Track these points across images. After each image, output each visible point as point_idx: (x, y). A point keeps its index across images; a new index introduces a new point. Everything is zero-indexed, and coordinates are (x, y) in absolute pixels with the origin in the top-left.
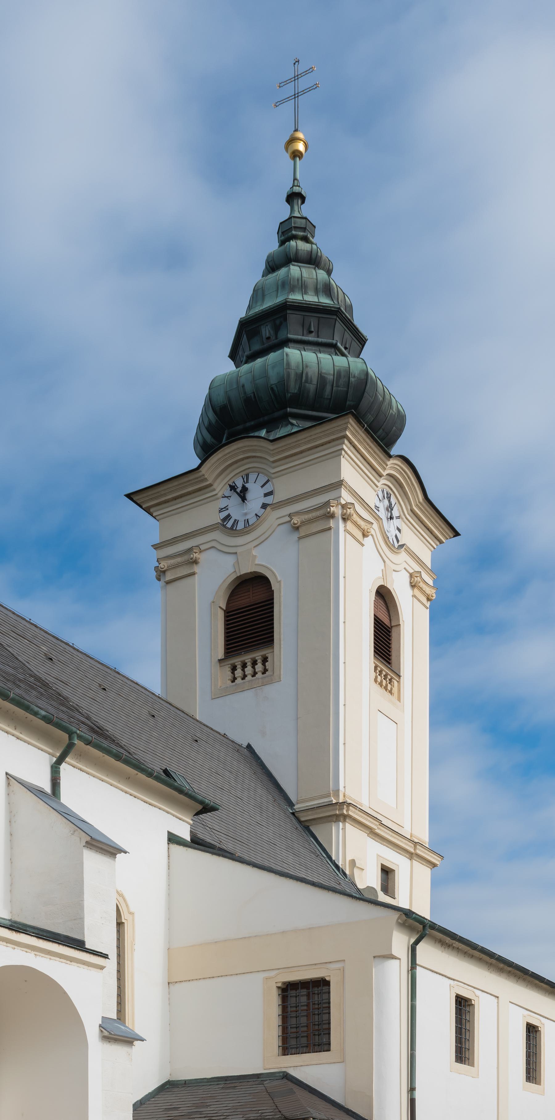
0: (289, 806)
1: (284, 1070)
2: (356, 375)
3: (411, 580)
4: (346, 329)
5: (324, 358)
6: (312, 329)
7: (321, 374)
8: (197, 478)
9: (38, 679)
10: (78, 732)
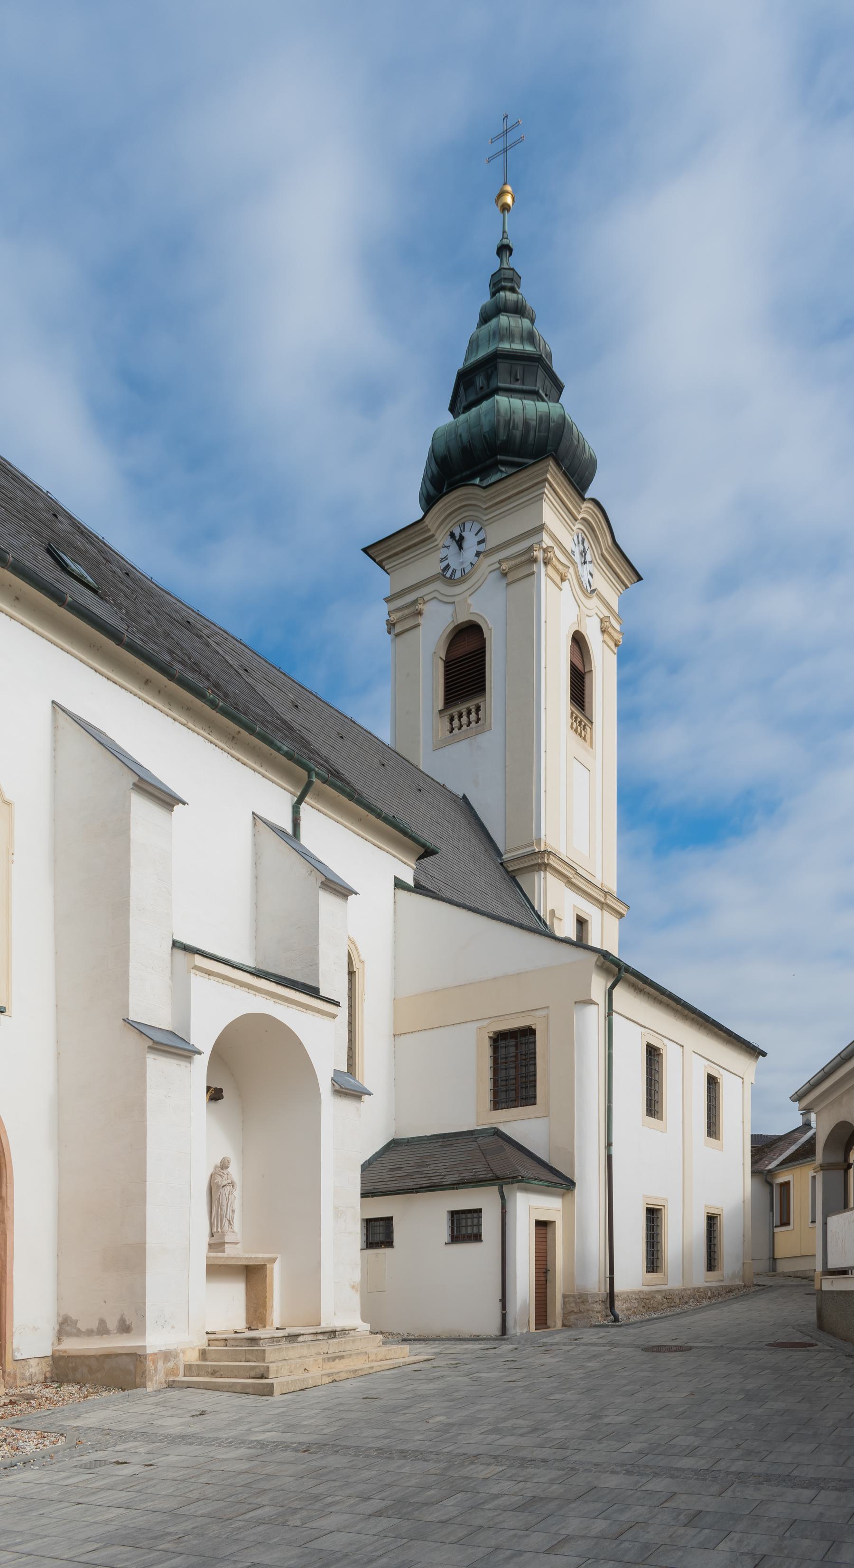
0: (498, 856)
1: (495, 1126)
2: (555, 419)
3: (601, 625)
4: (547, 376)
5: (528, 404)
6: (519, 377)
7: (526, 420)
8: (422, 529)
9: (284, 722)
10: (316, 769)
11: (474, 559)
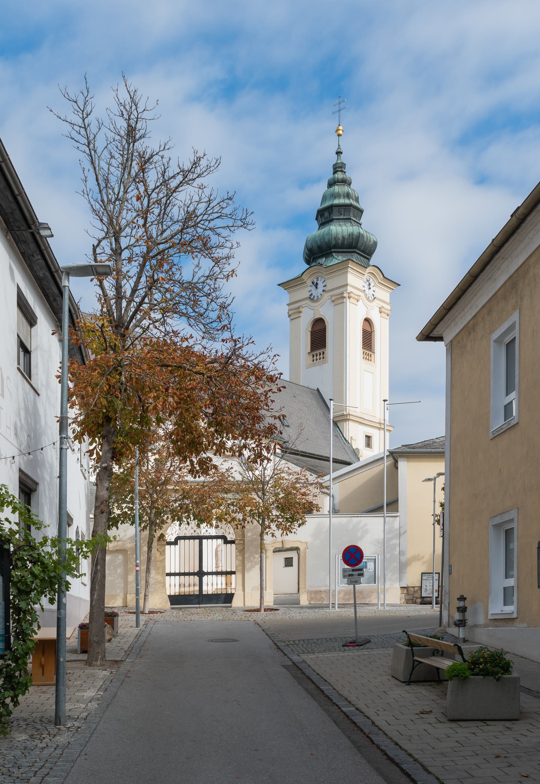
11: (321, 292)
